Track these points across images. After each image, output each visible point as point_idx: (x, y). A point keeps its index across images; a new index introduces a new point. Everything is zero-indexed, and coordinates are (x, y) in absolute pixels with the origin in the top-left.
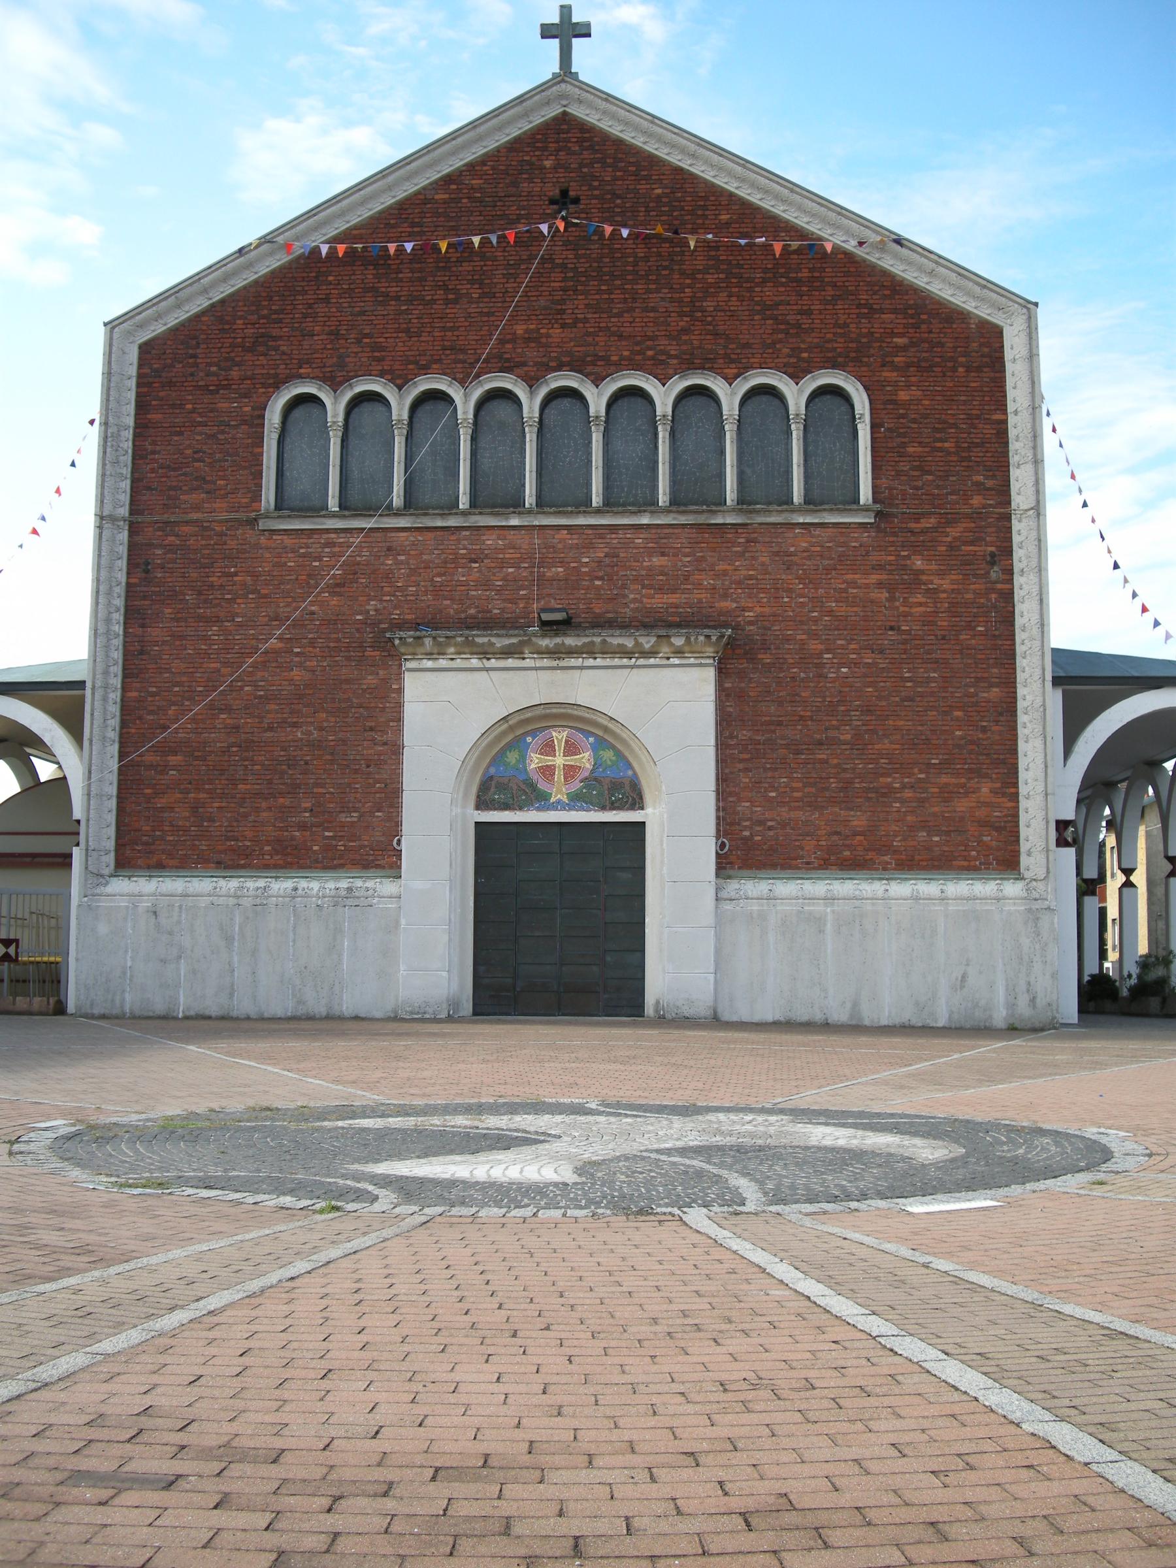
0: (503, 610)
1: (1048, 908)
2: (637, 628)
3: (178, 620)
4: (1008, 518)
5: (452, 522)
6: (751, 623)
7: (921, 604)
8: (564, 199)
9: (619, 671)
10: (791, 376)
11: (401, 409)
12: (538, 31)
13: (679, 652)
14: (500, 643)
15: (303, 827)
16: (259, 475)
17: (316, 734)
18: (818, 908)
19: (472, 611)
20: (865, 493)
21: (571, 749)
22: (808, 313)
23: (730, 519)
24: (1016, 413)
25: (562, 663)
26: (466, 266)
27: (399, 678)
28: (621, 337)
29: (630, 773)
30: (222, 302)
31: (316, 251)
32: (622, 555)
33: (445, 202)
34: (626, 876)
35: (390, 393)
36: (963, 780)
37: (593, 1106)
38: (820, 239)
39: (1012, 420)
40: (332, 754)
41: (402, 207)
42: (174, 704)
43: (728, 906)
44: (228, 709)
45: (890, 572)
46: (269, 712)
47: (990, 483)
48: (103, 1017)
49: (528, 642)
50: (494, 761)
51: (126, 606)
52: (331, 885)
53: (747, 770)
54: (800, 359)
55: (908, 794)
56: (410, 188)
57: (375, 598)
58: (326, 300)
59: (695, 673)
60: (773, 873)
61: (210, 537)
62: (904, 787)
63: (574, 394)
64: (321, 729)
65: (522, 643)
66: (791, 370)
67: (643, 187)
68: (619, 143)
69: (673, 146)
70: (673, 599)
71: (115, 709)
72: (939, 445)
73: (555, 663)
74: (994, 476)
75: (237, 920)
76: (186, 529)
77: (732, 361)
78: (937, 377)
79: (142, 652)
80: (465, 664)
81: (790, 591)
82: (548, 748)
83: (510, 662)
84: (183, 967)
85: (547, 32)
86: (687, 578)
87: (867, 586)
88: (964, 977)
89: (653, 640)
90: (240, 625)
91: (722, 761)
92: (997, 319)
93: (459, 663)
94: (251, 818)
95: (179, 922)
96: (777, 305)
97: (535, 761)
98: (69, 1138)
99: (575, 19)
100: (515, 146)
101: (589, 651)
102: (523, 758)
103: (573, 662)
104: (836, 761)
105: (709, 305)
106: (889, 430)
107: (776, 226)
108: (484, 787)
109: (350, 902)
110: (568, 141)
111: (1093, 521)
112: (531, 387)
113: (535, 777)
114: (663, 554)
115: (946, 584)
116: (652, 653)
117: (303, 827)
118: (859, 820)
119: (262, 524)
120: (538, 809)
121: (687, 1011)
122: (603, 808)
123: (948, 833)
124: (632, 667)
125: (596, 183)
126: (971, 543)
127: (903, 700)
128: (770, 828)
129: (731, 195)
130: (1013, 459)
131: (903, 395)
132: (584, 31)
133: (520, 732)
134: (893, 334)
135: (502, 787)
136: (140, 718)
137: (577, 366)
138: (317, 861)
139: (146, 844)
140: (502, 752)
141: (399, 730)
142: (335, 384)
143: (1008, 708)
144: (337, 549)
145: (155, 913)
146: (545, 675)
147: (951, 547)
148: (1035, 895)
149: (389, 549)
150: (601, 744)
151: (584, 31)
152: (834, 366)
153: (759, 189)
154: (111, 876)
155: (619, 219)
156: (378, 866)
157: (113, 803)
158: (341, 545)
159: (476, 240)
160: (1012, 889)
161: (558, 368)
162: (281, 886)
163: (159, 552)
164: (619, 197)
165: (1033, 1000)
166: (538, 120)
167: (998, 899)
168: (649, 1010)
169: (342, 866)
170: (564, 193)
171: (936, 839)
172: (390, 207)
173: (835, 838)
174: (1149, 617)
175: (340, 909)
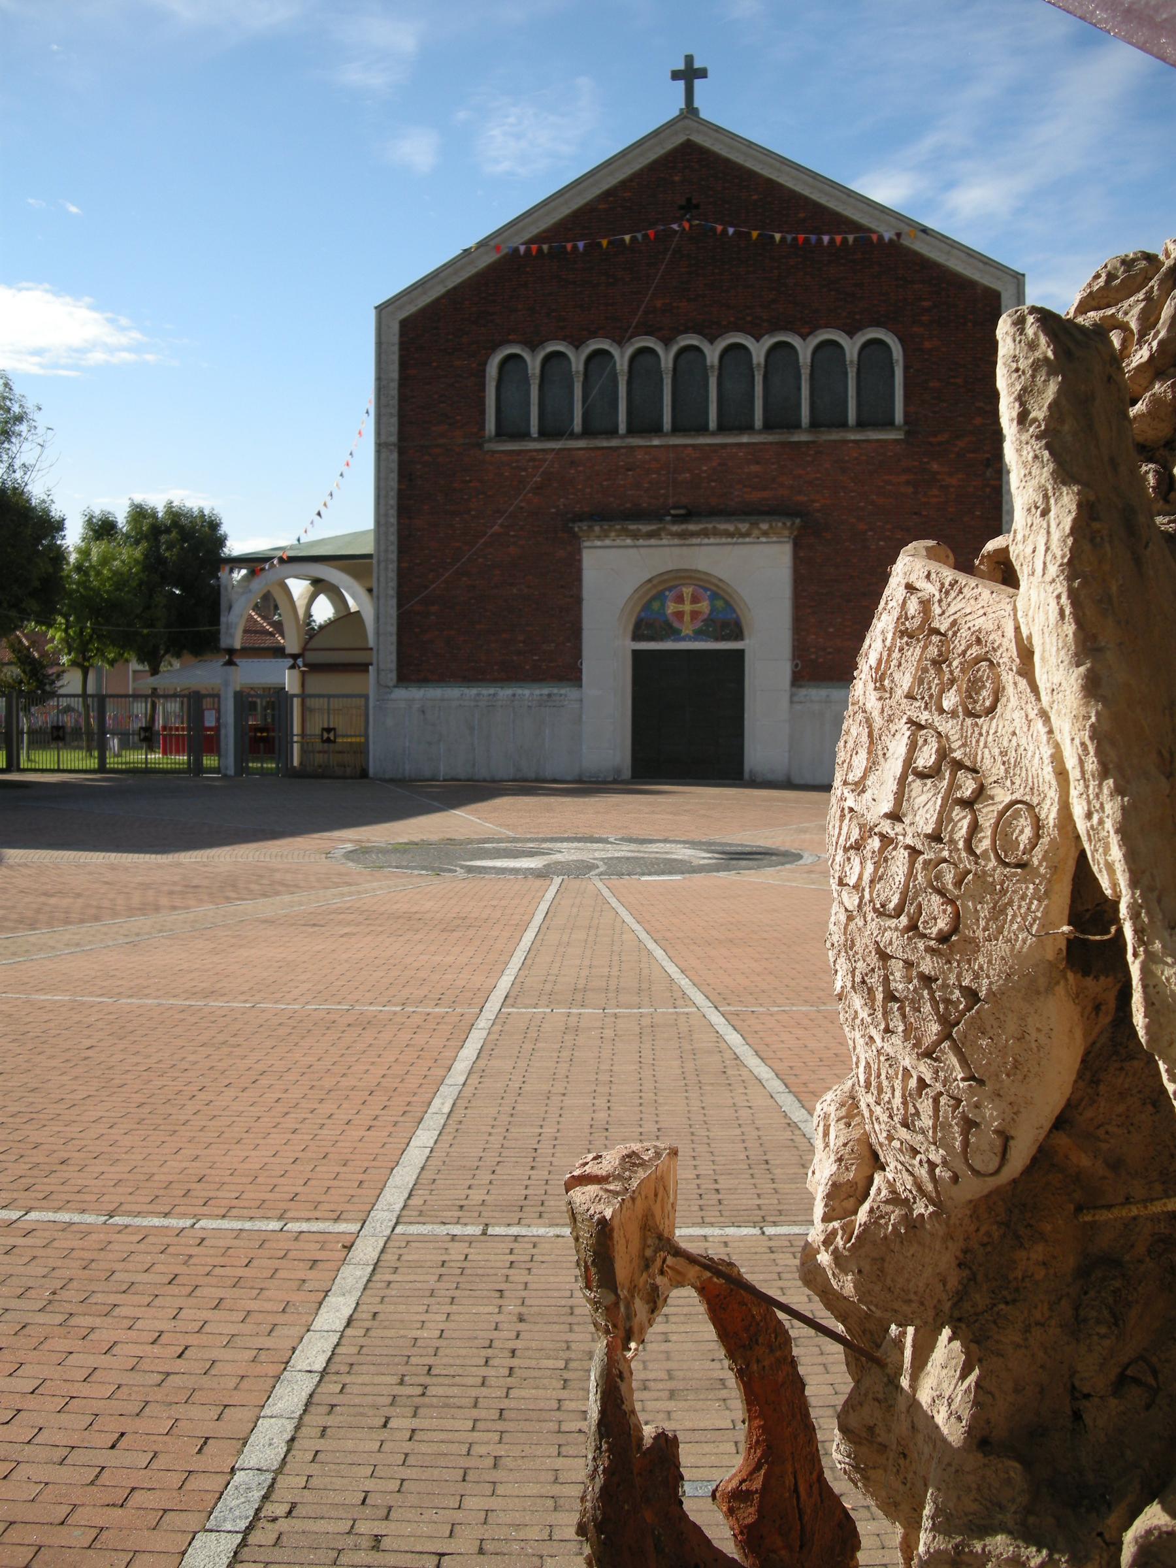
5: (614, 443)
7: (936, 496)
8: (689, 206)
9: (725, 547)
12: (669, 75)
13: (765, 534)
14: (645, 528)
16: (483, 412)
19: (628, 505)
20: (899, 417)
23: (803, 437)
25: (687, 542)
27: (579, 551)
30: (455, 288)
31: (516, 250)
37: (611, 840)
38: (870, 230)
43: (798, 707)
48: (392, 780)
49: (664, 529)
50: (647, 607)
52: (537, 692)
63: (697, 349)
65: (660, 529)
68: (727, 161)
71: (393, 575)
72: (952, 380)
73: (682, 542)
80: (622, 543)
82: (680, 599)
83: (653, 542)
85: (676, 75)
93: (618, 542)
97: (671, 608)
98: (351, 852)
99: (697, 65)
100: (654, 167)
101: (705, 533)
102: (663, 606)
107: (839, 222)
112: (666, 345)
113: (671, 619)
114: (758, 463)
116: (747, 534)
119: (488, 446)
120: (674, 641)
121: (770, 777)
122: (717, 639)
131: (927, 345)
132: (702, 73)
133: (661, 588)
137: (698, 330)
141: (579, 587)
142: (533, 347)
145: (423, 712)
146: (676, 550)
149: (572, 462)
150: (715, 596)
151: (702, 73)
154: (395, 687)
156: (568, 680)
157: (394, 639)
161: (685, 332)
162: (505, 693)
163: (419, 467)
168: (746, 776)
170: (689, 200)
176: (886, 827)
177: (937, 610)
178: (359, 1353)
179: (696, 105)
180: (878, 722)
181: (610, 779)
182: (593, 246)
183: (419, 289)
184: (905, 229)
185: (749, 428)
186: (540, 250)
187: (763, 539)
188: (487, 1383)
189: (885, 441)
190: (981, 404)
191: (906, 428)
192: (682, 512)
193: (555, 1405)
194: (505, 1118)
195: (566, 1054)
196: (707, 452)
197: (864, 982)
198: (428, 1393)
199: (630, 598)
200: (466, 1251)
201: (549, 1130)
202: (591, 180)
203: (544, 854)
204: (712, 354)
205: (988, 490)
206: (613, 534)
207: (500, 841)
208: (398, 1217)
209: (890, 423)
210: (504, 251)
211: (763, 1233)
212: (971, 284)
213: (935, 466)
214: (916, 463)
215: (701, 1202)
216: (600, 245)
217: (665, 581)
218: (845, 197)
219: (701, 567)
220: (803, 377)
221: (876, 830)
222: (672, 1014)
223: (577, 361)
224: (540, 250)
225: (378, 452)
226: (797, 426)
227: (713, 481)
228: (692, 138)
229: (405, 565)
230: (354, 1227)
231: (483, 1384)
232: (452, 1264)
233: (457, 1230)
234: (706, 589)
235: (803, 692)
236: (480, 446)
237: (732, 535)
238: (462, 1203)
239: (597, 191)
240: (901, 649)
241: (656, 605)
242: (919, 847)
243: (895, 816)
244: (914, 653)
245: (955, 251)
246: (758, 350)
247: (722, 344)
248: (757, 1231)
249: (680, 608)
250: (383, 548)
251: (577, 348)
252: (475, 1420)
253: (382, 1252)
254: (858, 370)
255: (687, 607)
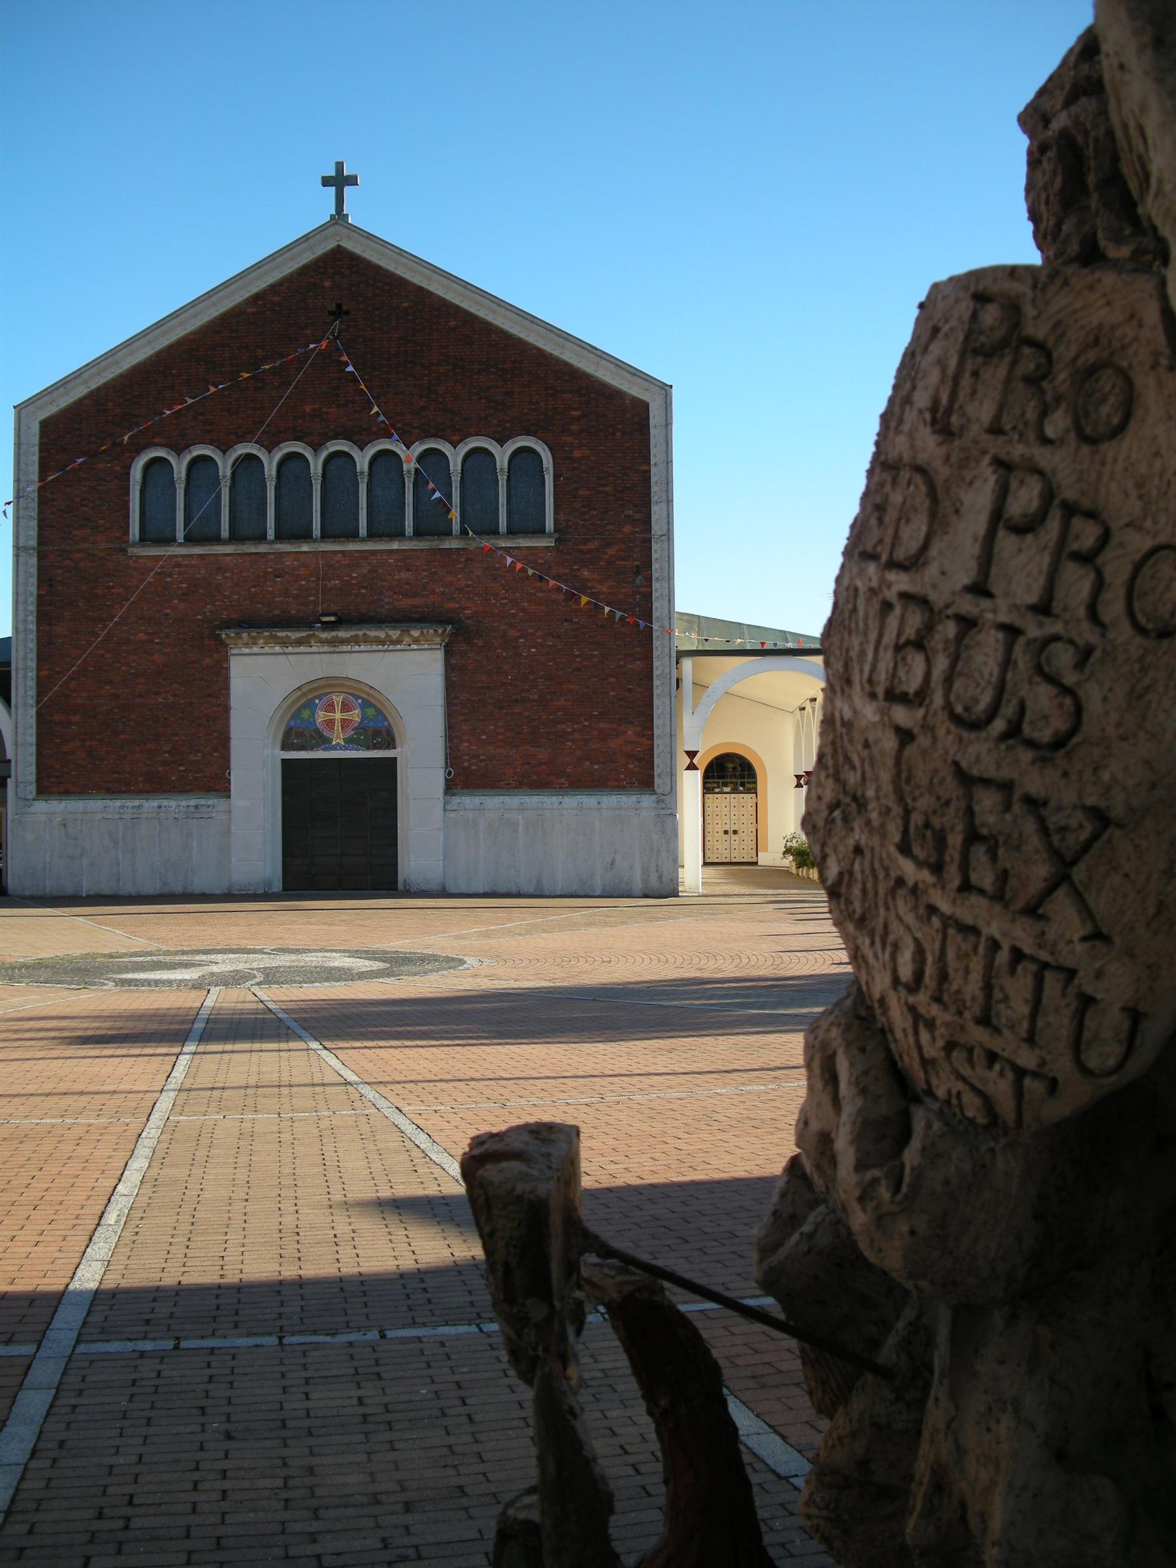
13: (416, 641)
14: (295, 635)
19: (277, 612)
20: (550, 525)
21: (346, 708)
25: (287, 650)
27: (227, 659)
30: (98, 389)
50: (293, 717)
52: (184, 803)
55: (577, 736)
65: (309, 636)
68: (378, 267)
70: (416, 601)
73: (332, 649)
82: (331, 708)
83: (302, 649)
85: (326, 182)
88: (613, 862)
97: (321, 716)
100: (304, 271)
101: (355, 640)
108: (288, 733)
109: (197, 815)
114: (408, 570)
116: (398, 642)
119: (132, 551)
120: (324, 750)
121: (424, 886)
122: (368, 748)
132: (352, 181)
135: (300, 734)
142: (179, 451)
150: (366, 704)
151: (352, 181)
152: (528, 434)
156: (216, 790)
157: (33, 749)
162: (150, 805)
163: (59, 572)
165: (660, 877)
168: (400, 886)
170: (339, 306)
176: (967, 605)
177: (1029, 311)
178: (47, 1487)
180: (942, 472)
183: (61, 390)
185: (400, 535)
188: (198, 1509)
189: (536, 548)
191: (557, 535)
192: (332, 619)
193: (279, 1528)
194: (184, 1228)
195: (243, 1159)
196: (357, 559)
197: (927, 825)
198: (132, 1526)
200: (159, 1367)
201: (234, 1237)
202: (240, 283)
203: (199, 965)
204: (362, 460)
207: (150, 954)
208: (79, 1335)
209: (541, 531)
211: (481, 1330)
212: (620, 394)
213: (586, 574)
215: (410, 1302)
217: (315, 689)
221: (950, 612)
222: (350, 1116)
223: (225, 465)
225: (17, 556)
226: (448, 533)
230: (29, 1349)
231: (194, 1511)
232: (144, 1383)
233: (148, 1346)
234: (357, 697)
235: (456, 800)
236: (124, 551)
237: (383, 643)
238: (148, 1317)
239: (246, 294)
240: (975, 374)
242: (1018, 623)
243: (980, 589)
244: (995, 374)
247: (372, 450)
248: (474, 1329)
251: (224, 452)
252: (190, 1553)
253: (63, 1374)
254: (508, 477)
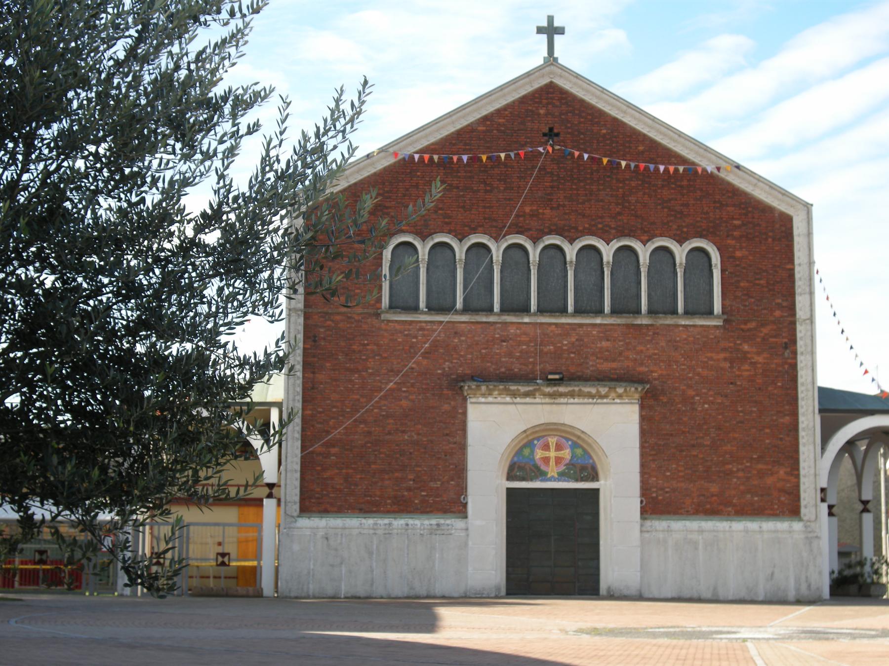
0: (520, 370)
1: (817, 537)
2: (593, 381)
3: (334, 370)
4: (793, 324)
5: (492, 319)
6: (656, 379)
7: (747, 370)
8: (551, 134)
10: (678, 241)
11: (461, 253)
13: (620, 396)
14: (523, 389)
15: (409, 489)
17: (415, 437)
18: (694, 536)
19: (503, 370)
20: (717, 307)
22: (687, 205)
23: (644, 321)
24: (800, 265)
25: (556, 401)
26: (497, 171)
28: (584, 216)
29: (591, 461)
30: (355, 184)
31: (412, 157)
32: (586, 340)
33: (483, 132)
34: (588, 518)
35: (454, 244)
36: (770, 467)
38: (693, 164)
39: (797, 269)
40: (425, 448)
41: (459, 133)
42: (333, 418)
43: (646, 535)
44: (364, 422)
45: (731, 352)
46: (389, 424)
47: (785, 304)
49: (539, 390)
50: (519, 452)
51: (303, 361)
52: (426, 522)
53: (654, 460)
54: (682, 232)
55: (741, 474)
56: (464, 123)
57: (448, 361)
58: (417, 186)
59: (628, 408)
60: (668, 517)
61: (352, 323)
62: (738, 470)
64: (418, 434)
65: (535, 390)
66: (677, 238)
67: (595, 128)
68: (582, 102)
69: (613, 106)
70: (614, 365)
72: (757, 282)
73: (552, 401)
74: (787, 300)
75: (375, 542)
76: (338, 317)
77: (645, 232)
78: (757, 241)
79: (313, 388)
81: (676, 362)
82: (546, 447)
83: (528, 400)
84: (344, 569)
85: (540, 30)
86: (620, 354)
87: (718, 360)
88: (773, 574)
89: (607, 389)
90: (371, 374)
91: (643, 455)
92: (789, 211)
93: (499, 399)
94: (379, 484)
95: (341, 543)
96: (670, 200)
97: (539, 454)
100: (523, 100)
101: (572, 395)
103: (562, 400)
104: (702, 456)
105: (633, 199)
106: (730, 273)
109: (438, 532)
110: (552, 99)
111: (828, 298)
112: (534, 243)
113: (539, 463)
114: (608, 340)
115: (760, 359)
117: (409, 489)
118: (714, 488)
119: (383, 317)
120: (541, 481)
121: (626, 592)
122: (577, 480)
123: (762, 496)
124: (595, 404)
125: (569, 125)
126: (775, 337)
127: (738, 422)
128: (667, 492)
129: (645, 135)
130: (798, 290)
131: (738, 254)
132: (561, 31)
133: (531, 438)
134: (733, 219)
135: (521, 468)
136: (313, 426)
137: (560, 232)
138: (417, 509)
139: (318, 498)
140: (521, 450)
143: (794, 428)
144: (426, 332)
145: (327, 538)
146: (547, 408)
147: (764, 339)
148: (809, 529)
149: (456, 333)
150: (575, 445)
151: (561, 31)
153: (661, 133)
155: (582, 147)
156: (451, 512)
157: (298, 475)
158: (428, 330)
159: (503, 155)
160: (797, 526)
161: (549, 233)
162: (399, 523)
163: (322, 330)
164: (583, 134)
165: (809, 586)
166: (536, 85)
167: (790, 532)
169: (431, 512)
170: (551, 129)
171: (756, 499)
172: (453, 133)
173: (702, 498)
174: (869, 377)
175: (434, 536)
179: (555, 56)
181: (493, 595)
182: (475, 159)
184: (723, 164)
185: (600, 312)
186: (431, 159)
187: (618, 401)
189: (708, 326)
190: (780, 301)
199: (509, 446)
204: (571, 252)
205: (786, 367)
206: (496, 393)
210: (400, 157)
213: (746, 347)
214: (732, 345)
216: (481, 160)
217: (536, 432)
218: (676, 136)
219: (567, 421)
220: (643, 275)
224: (431, 159)
227: (572, 353)
228: (554, 81)
229: (309, 412)
234: (567, 439)
235: (648, 523)
236: (378, 315)
241: (526, 452)
245: (761, 184)
246: (608, 251)
249: (547, 454)
250: (291, 397)
251: (461, 240)
255: (552, 454)
